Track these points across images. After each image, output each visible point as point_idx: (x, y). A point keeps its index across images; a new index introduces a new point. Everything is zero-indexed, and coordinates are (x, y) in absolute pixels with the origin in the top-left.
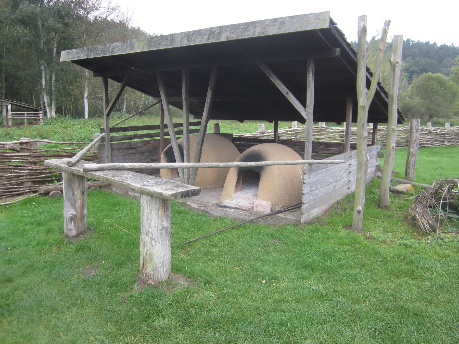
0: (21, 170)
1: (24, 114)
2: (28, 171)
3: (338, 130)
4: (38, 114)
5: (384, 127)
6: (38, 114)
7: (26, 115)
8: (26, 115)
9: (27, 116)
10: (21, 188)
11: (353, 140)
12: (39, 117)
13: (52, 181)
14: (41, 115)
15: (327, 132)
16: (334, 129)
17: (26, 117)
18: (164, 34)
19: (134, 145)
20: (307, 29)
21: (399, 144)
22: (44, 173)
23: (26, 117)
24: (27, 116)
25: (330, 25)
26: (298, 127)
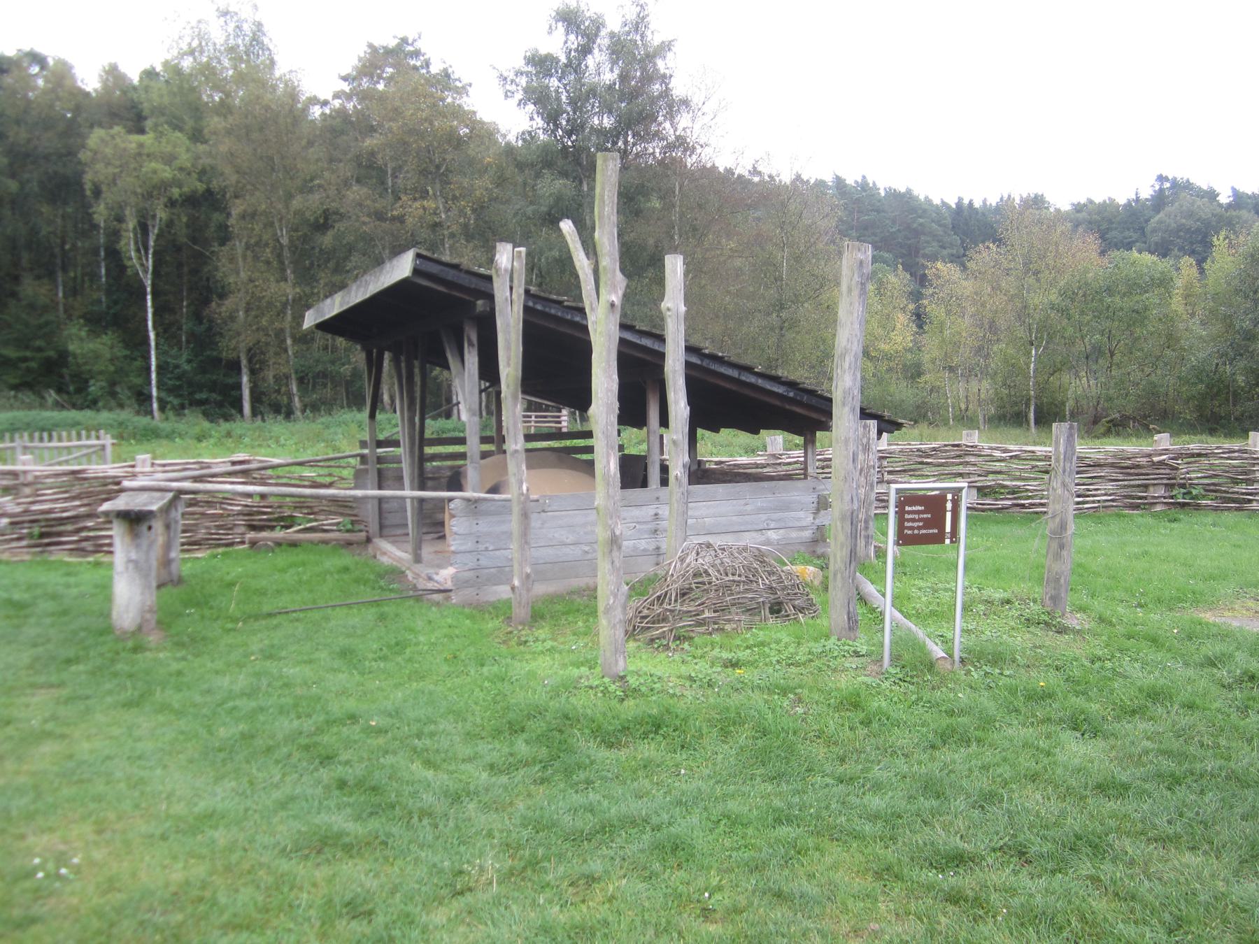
0: (231, 505)
1: (530, 417)
2: (239, 508)
3: (1033, 452)
4: (559, 417)
5: (1218, 448)
6: (559, 417)
7: (533, 418)
8: (533, 418)
9: (536, 422)
10: (228, 534)
11: (1095, 481)
12: (560, 422)
13: (272, 528)
14: (565, 418)
15: (987, 458)
16: (1012, 451)
17: (533, 424)
18: (921, 192)
19: (433, 473)
20: (351, 304)
21: (826, 478)
22: (265, 513)
23: (533, 424)
24: (536, 422)
25: (493, 289)
26: (889, 445)
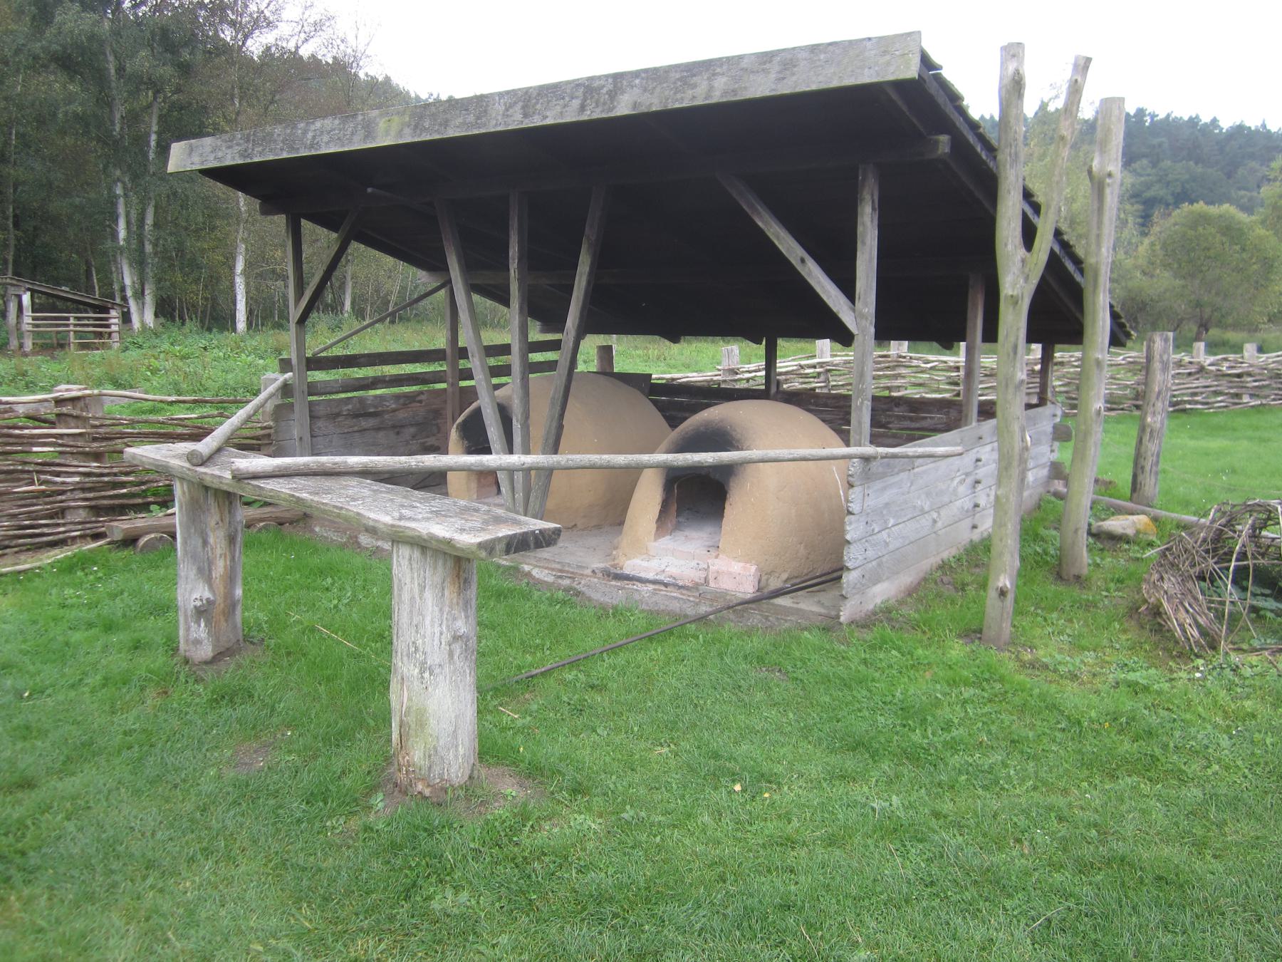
0: (58, 474)
1: (68, 319)
2: (77, 479)
3: (945, 362)
4: (107, 319)
5: (1071, 356)
6: (107, 319)
7: (72, 321)
8: (72, 321)
9: (76, 325)
10: (58, 525)
11: (986, 391)
12: (108, 326)
13: (145, 507)
14: (116, 321)
15: (914, 369)
16: (933, 361)
17: (71, 328)
18: (458, 96)
19: (376, 407)
21: (1115, 403)
22: (123, 485)
23: (71, 328)
24: (76, 325)
25: (920, 69)
26: (832, 356)
